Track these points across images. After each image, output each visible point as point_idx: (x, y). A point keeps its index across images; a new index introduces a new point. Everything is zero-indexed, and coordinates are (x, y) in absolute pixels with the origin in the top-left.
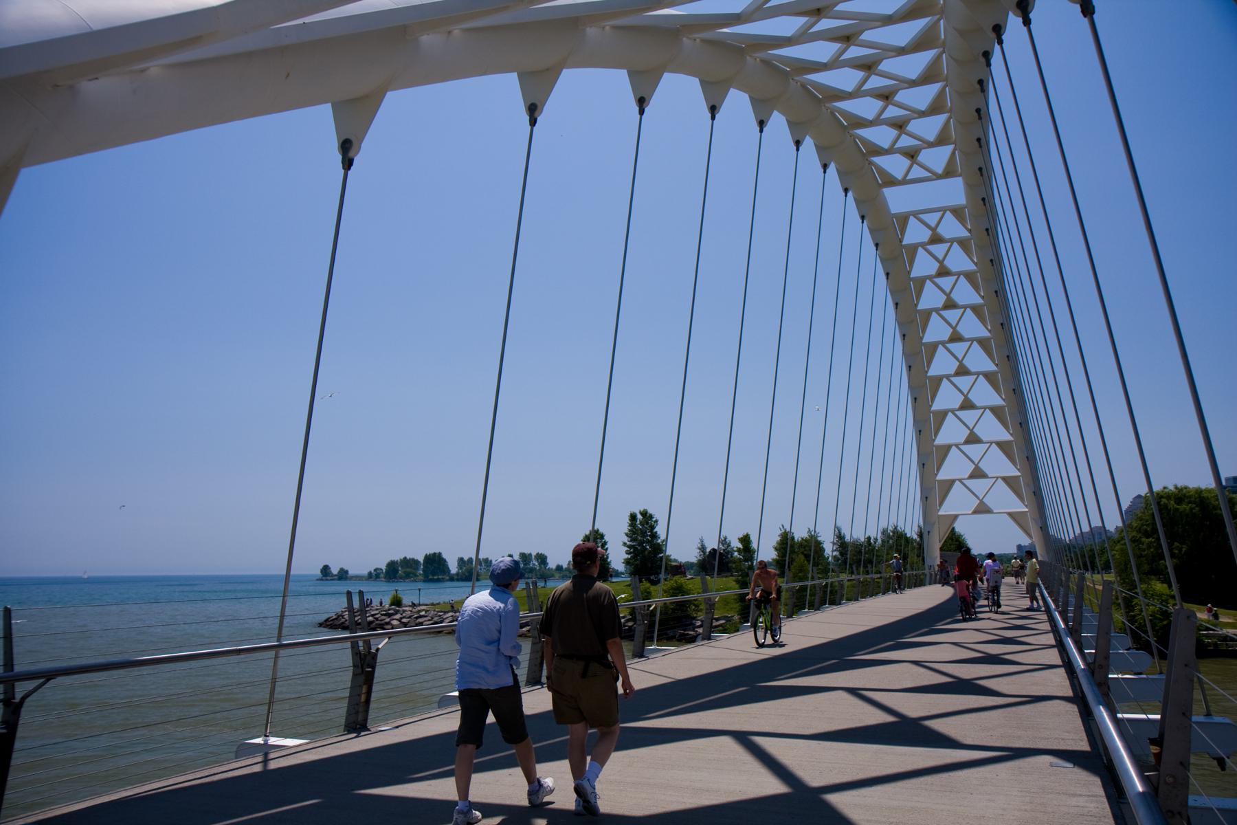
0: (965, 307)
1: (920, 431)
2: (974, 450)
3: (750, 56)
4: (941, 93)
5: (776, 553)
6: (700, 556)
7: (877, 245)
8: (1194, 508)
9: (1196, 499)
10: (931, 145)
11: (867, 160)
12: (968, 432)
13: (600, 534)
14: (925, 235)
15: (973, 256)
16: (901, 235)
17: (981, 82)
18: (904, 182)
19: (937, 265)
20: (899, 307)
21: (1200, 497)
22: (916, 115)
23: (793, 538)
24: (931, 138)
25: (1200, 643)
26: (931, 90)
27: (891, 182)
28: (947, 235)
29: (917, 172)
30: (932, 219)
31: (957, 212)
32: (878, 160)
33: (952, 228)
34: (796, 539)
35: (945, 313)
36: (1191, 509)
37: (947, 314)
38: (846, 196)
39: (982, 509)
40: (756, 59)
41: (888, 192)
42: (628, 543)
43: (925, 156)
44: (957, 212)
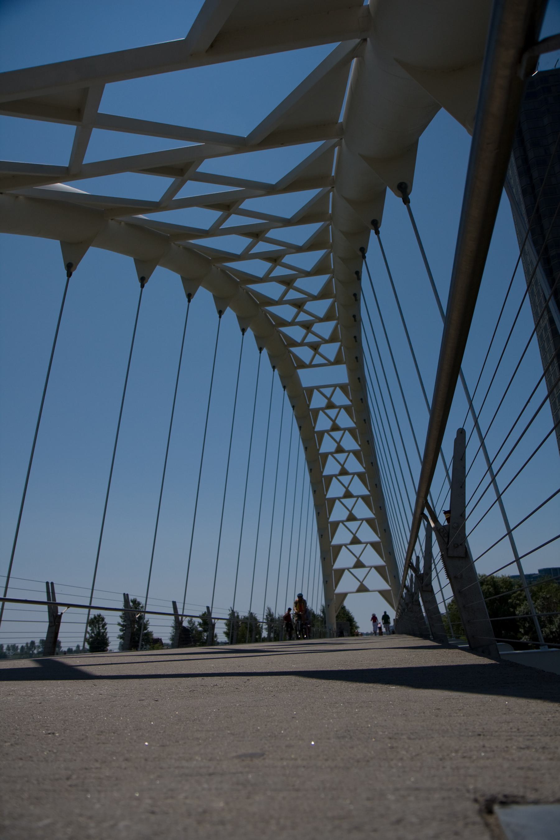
0: (358, 497)
1: (322, 535)
2: (360, 573)
3: (214, 265)
4: (329, 282)
5: (227, 627)
6: (173, 632)
7: (293, 407)
8: (490, 588)
9: (490, 582)
10: (321, 320)
11: (287, 349)
12: (359, 584)
13: (102, 618)
14: (323, 403)
15: (363, 464)
16: (309, 402)
17: (355, 295)
18: (311, 366)
19: (335, 445)
20: (312, 471)
21: (493, 581)
22: (311, 299)
23: (238, 616)
24: (321, 315)
25: (450, 513)
26: (322, 280)
27: (303, 365)
28: (338, 403)
29: (318, 360)
30: (328, 392)
31: (343, 388)
32: (293, 349)
33: (340, 399)
34: (240, 617)
35: (332, 433)
36: (488, 589)
37: (349, 524)
38: (274, 371)
39: (362, 589)
40: (218, 268)
41: (301, 373)
42: (122, 623)
43: (323, 349)
44: (343, 388)
